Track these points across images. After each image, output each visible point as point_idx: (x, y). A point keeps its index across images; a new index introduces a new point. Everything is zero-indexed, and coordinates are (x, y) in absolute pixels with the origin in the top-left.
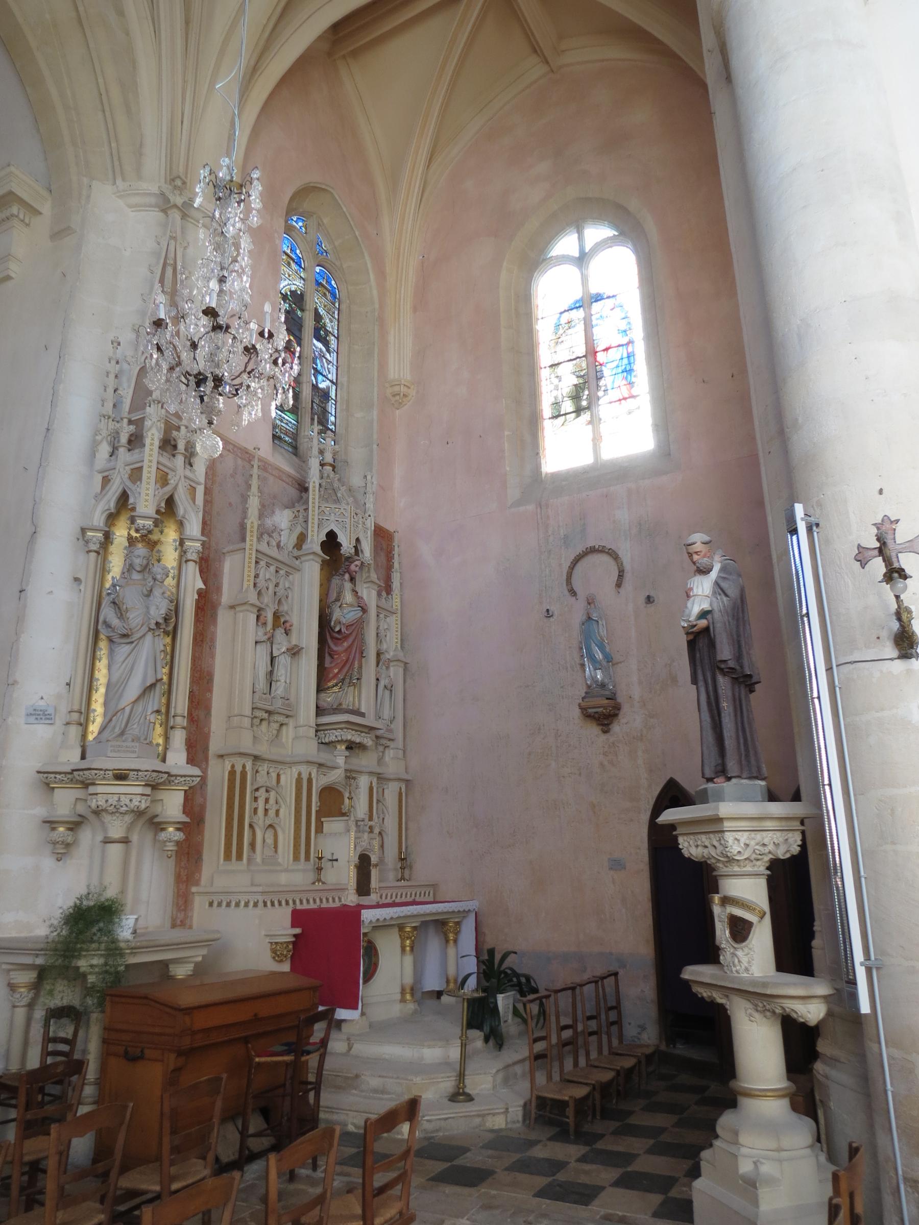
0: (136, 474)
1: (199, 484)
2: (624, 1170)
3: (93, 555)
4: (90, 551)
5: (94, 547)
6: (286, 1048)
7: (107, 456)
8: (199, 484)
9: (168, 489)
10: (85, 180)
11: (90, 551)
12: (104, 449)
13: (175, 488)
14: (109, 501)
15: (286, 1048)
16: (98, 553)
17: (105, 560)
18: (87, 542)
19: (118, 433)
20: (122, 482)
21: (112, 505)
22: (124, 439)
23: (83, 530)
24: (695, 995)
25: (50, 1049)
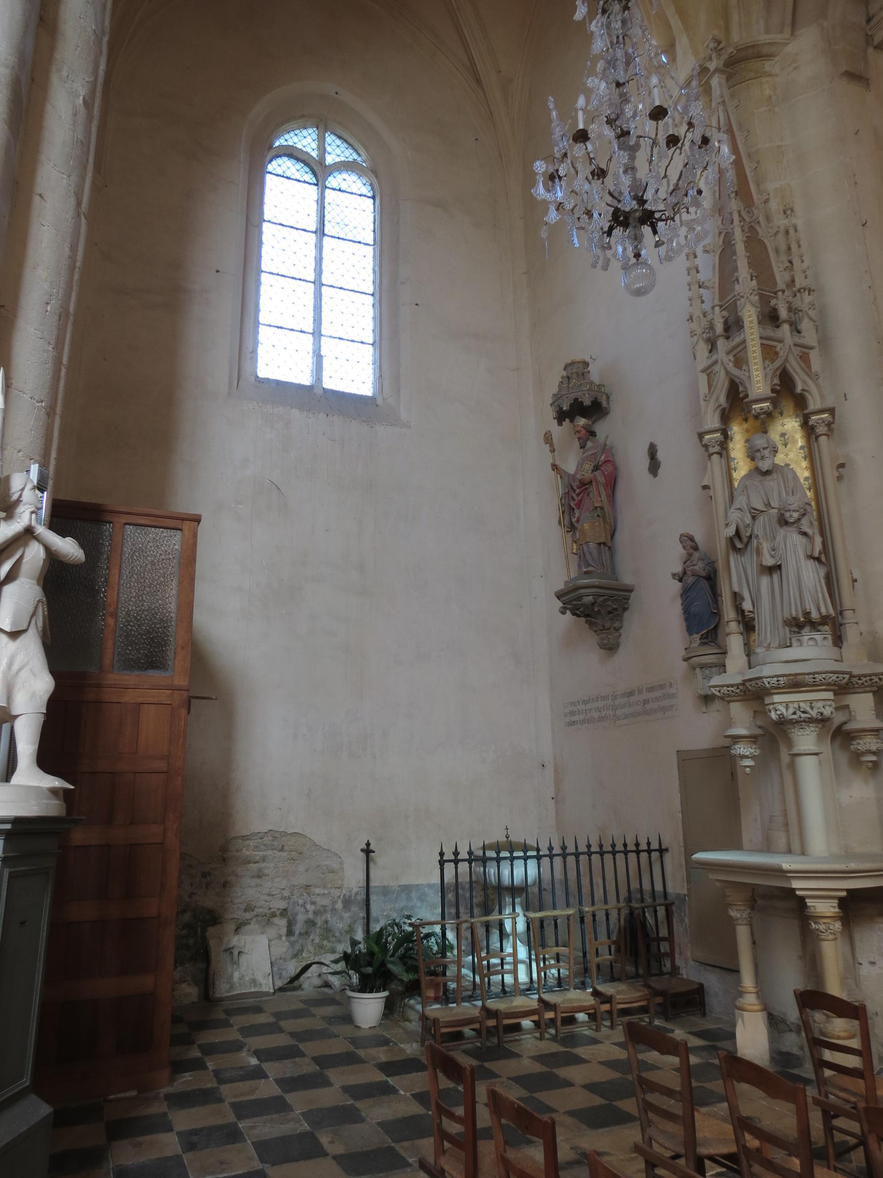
0: (740, 361)
1: (812, 348)
2: (390, 1080)
3: (715, 457)
4: (713, 454)
5: (717, 449)
6: (598, 1101)
7: (706, 353)
8: (812, 348)
9: (778, 363)
10: (378, 983)
11: (713, 454)
12: (703, 348)
13: (786, 360)
14: (717, 399)
15: (598, 1101)
16: (720, 454)
17: (728, 459)
18: (706, 446)
19: (712, 324)
20: (727, 373)
21: (723, 400)
22: (719, 328)
23: (701, 436)
24: (82, 545)
25: (658, 908)
